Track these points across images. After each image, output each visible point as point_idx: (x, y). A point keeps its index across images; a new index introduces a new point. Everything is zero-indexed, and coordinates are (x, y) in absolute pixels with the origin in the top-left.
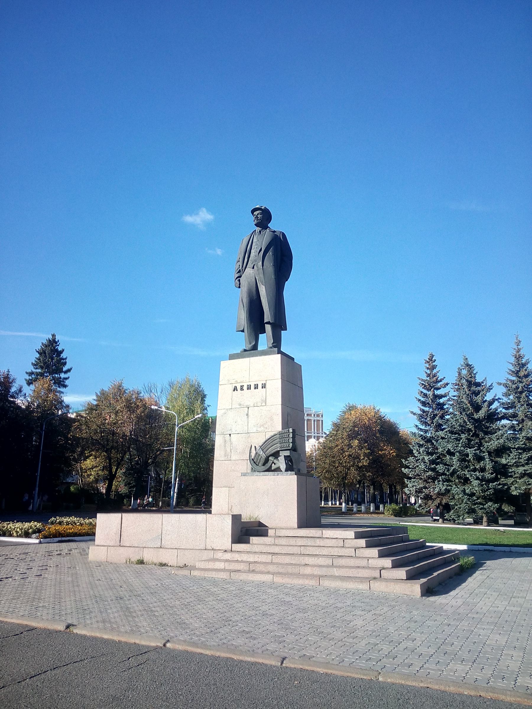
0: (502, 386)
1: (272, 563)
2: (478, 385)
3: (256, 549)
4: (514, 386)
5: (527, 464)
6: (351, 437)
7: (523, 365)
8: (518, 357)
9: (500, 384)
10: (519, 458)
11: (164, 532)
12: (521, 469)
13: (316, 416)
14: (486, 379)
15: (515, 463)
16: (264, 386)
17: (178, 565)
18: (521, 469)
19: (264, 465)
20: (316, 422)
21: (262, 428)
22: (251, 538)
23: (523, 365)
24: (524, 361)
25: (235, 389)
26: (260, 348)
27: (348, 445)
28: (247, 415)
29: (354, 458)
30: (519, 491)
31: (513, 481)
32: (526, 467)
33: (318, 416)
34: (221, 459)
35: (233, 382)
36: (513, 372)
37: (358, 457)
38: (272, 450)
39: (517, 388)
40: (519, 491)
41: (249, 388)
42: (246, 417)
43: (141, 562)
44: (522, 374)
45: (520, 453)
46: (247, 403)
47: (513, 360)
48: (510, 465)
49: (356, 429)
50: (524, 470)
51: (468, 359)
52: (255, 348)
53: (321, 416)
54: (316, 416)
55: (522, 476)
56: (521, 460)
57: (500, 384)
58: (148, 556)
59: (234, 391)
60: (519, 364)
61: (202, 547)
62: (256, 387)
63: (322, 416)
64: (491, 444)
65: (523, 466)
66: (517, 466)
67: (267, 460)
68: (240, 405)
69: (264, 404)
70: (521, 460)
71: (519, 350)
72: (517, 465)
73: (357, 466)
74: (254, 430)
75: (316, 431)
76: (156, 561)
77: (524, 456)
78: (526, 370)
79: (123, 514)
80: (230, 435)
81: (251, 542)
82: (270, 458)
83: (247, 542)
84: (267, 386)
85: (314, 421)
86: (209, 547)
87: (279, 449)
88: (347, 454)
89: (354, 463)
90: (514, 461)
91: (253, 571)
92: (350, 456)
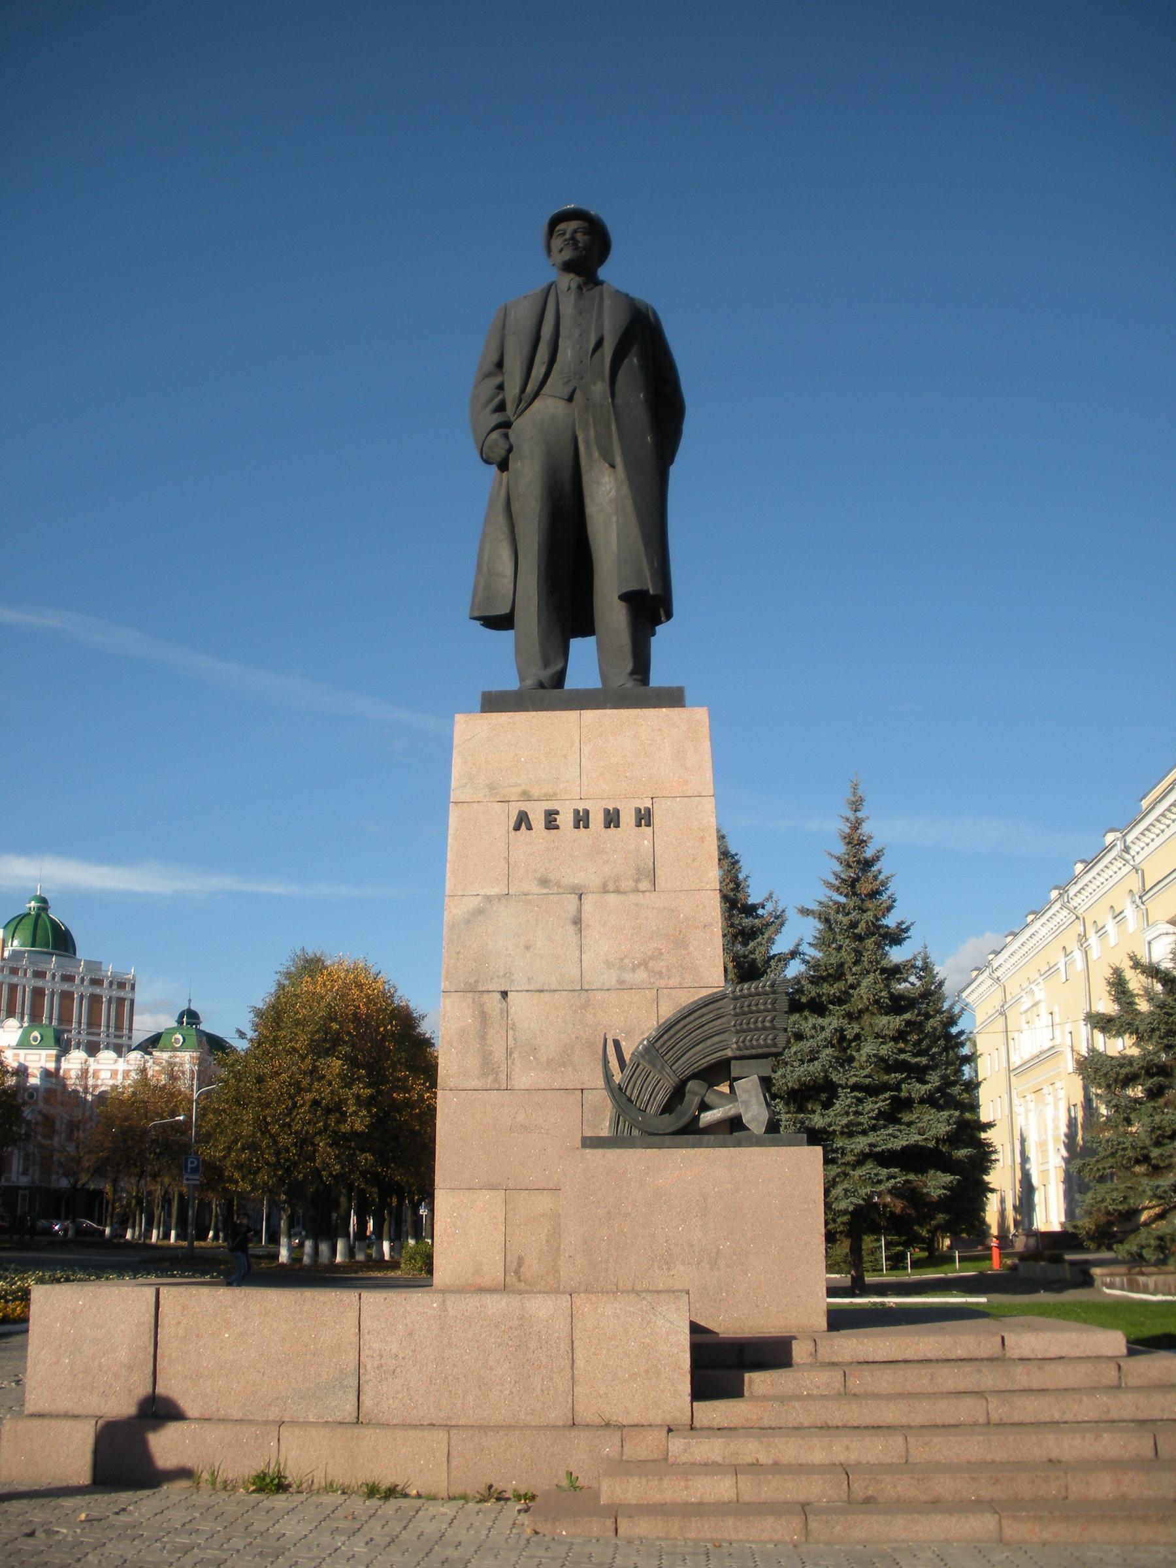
0: (810, 918)
1: (906, 1466)
2: (750, 910)
3: (765, 1414)
4: (845, 920)
5: (874, 1128)
6: (326, 1044)
7: (868, 864)
8: (856, 842)
9: (805, 912)
10: (857, 1113)
11: (369, 1363)
12: (861, 1143)
13: (115, 987)
14: (770, 896)
15: (847, 1126)
16: (644, 818)
17: (457, 1490)
18: (861, 1143)
19: (668, 1108)
20: (113, 1007)
21: (641, 976)
22: (747, 1376)
23: (868, 864)
24: (869, 853)
25: (523, 821)
26: (570, 683)
27: (311, 1072)
28: (577, 921)
29: (328, 1111)
30: (854, 1200)
31: (838, 1175)
32: (872, 1138)
33: (121, 985)
34: (467, 1085)
35: (513, 793)
36: (844, 881)
37: (337, 1108)
38: (700, 1056)
39: (854, 925)
40: (854, 1200)
41: (612, 819)
42: (571, 929)
43: (272, 1484)
44: (864, 888)
45: (860, 1101)
46: (578, 879)
47: (841, 849)
48: (834, 1131)
49: (335, 1026)
50: (871, 1145)
51: (727, 839)
52: (559, 680)
53: (128, 988)
54: (115, 987)
55: (863, 1159)
56: (861, 1119)
57: (805, 912)
58: (300, 1457)
59: (517, 828)
60: (858, 862)
61: (557, 1415)
62: (582, 819)
63: (133, 987)
64: (784, 1076)
65: (864, 1133)
66: (851, 1135)
67: (678, 1094)
68: (544, 882)
69: (645, 885)
70: (861, 1119)
71: (856, 825)
72: (849, 1132)
73: (335, 1132)
74: (611, 978)
75: (112, 1030)
76: (341, 1474)
77: (867, 1109)
78: (875, 878)
79: (168, 1294)
80: (504, 994)
81: (746, 1393)
82: (691, 1085)
83: (734, 1391)
84: (657, 819)
85: (110, 1001)
86: (586, 1414)
87: (729, 1053)
88: (309, 1096)
89: (326, 1126)
90: (845, 1121)
91: (868, 1500)
92: (316, 1103)
